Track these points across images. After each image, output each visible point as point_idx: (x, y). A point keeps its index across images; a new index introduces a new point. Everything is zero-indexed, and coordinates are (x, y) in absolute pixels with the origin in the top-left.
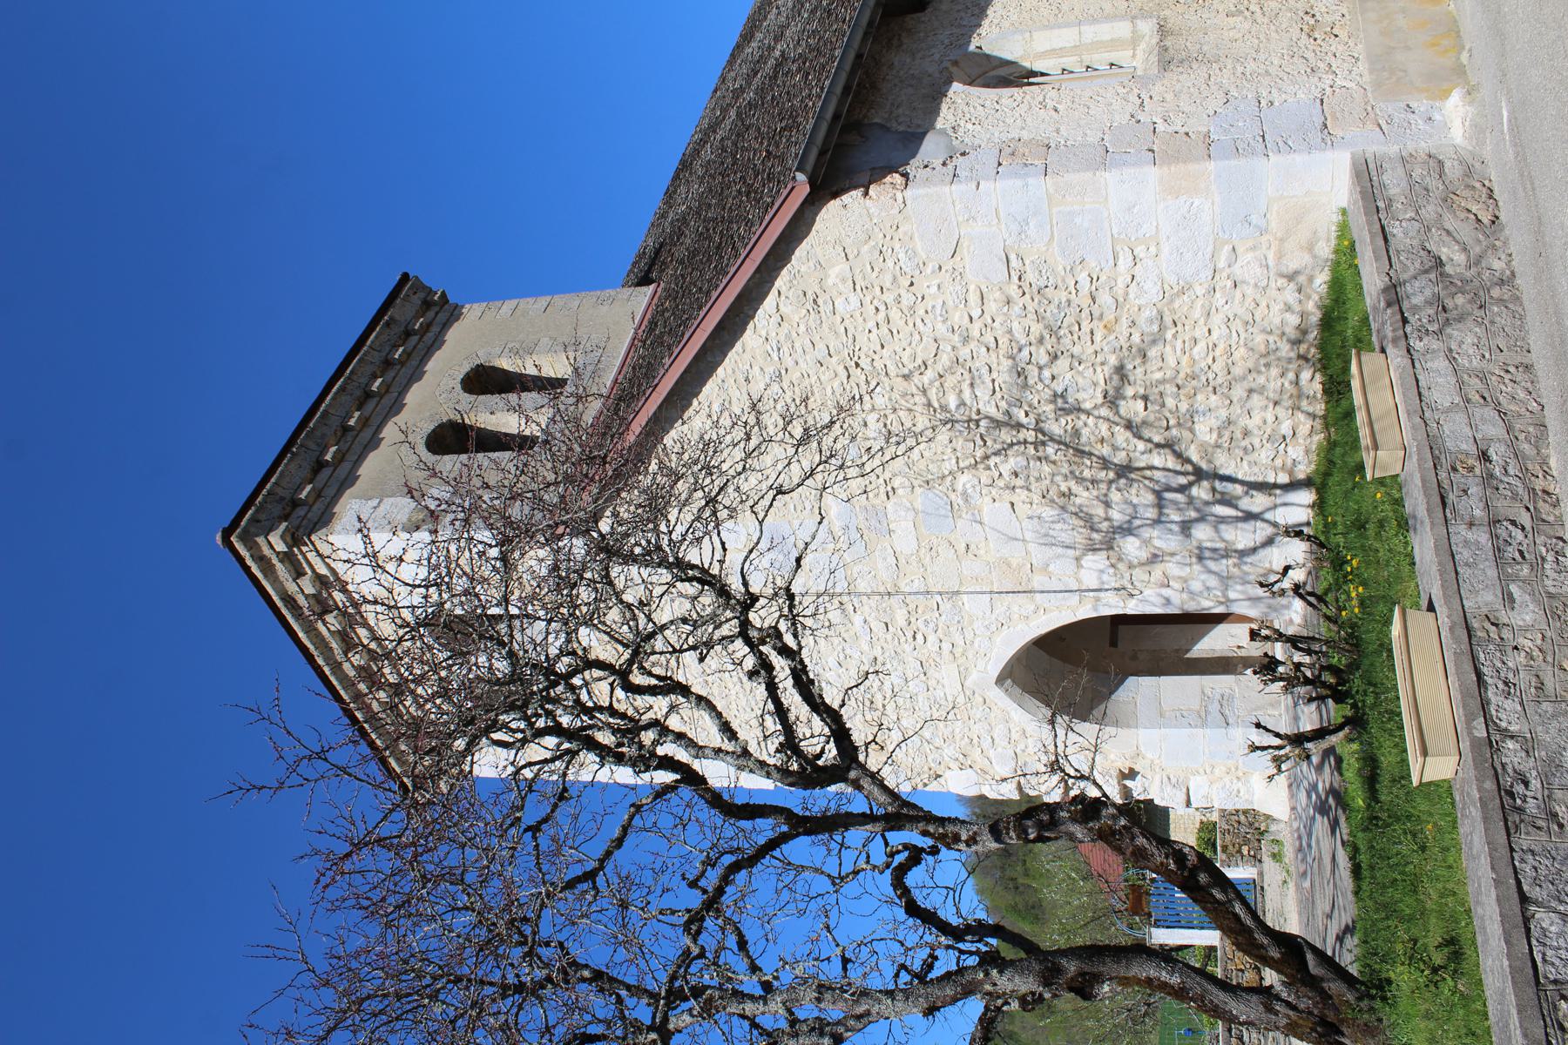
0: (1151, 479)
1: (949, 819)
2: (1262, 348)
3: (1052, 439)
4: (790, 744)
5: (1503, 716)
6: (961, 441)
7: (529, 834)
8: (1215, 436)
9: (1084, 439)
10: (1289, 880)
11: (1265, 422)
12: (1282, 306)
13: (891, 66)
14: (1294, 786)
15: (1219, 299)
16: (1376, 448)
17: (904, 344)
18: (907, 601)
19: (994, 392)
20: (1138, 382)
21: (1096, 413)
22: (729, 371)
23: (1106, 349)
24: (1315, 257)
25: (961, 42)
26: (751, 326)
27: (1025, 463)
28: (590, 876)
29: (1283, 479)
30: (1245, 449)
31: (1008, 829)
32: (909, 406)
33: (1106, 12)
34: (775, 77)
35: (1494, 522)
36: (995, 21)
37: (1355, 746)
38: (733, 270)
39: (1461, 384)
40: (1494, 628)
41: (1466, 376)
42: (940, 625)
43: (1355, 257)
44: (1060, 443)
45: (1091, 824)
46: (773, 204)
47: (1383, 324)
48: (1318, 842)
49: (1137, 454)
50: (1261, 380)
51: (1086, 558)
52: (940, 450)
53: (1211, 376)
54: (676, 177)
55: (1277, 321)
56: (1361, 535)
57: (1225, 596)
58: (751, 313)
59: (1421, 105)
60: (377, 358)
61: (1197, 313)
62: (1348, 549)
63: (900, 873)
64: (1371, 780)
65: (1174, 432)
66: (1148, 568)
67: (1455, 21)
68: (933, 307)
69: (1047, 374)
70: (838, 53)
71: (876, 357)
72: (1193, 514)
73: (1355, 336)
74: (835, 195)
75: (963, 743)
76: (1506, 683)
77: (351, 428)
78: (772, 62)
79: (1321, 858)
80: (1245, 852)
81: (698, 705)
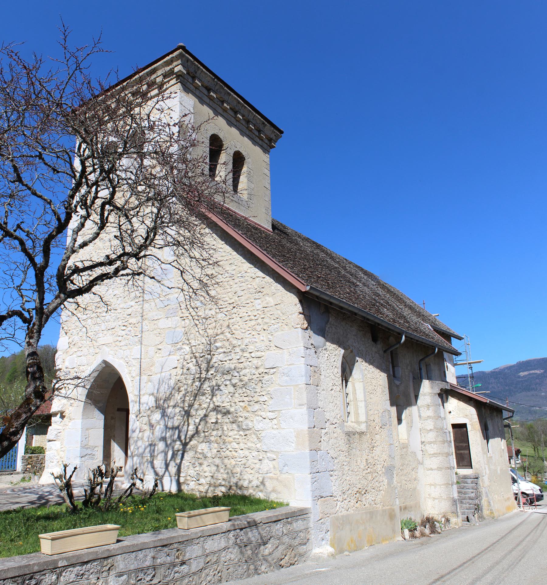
0: (184, 425)
1: (40, 335)
2: (234, 471)
3: (201, 384)
4: (77, 270)
5: (67, 574)
6: (202, 347)
7: (38, 154)
8: (200, 451)
9: (201, 397)
10: (12, 485)
11: (205, 472)
12: (251, 479)
13: (351, 327)
14: (53, 486)
15: (255, 453)
16: (189, 517)
17: (241, 326)
18: (139, 324)
19: (222, 361)
20: (223, 420)
21: (211, 403)
22: (234, 257)
23: (237, 407)
24: (270, 493)
25: (360, 355)
26: (252, 266)
27: (192, 373)
28: (19, 179)
29: (182, 480)
30: (194, 464)
31: (33, 359)
32: (217, 327)
33: (369, 412)
34: (349, 282)
35: (154, 568)
36: (367, 368)
37: (64, 510)
38: (274, 260)
39: (214, 553)
40: (107, 568)
41: (217, 555)
42: (129, 336)
43: (269, 509)
44: (200, 387)
45: (33, 395)
46: (299, 277)
47: (241, 520)
48: (26, 496)
49: (194, 419)
50: (222, 471)
51: (153, 398)
52: (199, 339)
53: (224, 450)
54: (314, 243)
55: (245, 477)
56: (154, 511)
57: (135, 455)
58: (257, 266)
59: (329, 536)
60: (251, 118)
61: (250, 444)
62: (149, 506)
63: (20, 315)
64: (47, 518)
65: (202, 434)
66: (148, 423)
67: (361, 549)
68: (255, 338)
69: (228, 383)
70: (356, 305)
71: (237, 315)
72: (169, 442)
73: (237, 509)
74: (300, 301)
75: (79, 344)
76: (82, 575)
77: (223, 104)
78: (355, 281)
79: (19, 497)
80: (28, 466)
81: (95, 233)
